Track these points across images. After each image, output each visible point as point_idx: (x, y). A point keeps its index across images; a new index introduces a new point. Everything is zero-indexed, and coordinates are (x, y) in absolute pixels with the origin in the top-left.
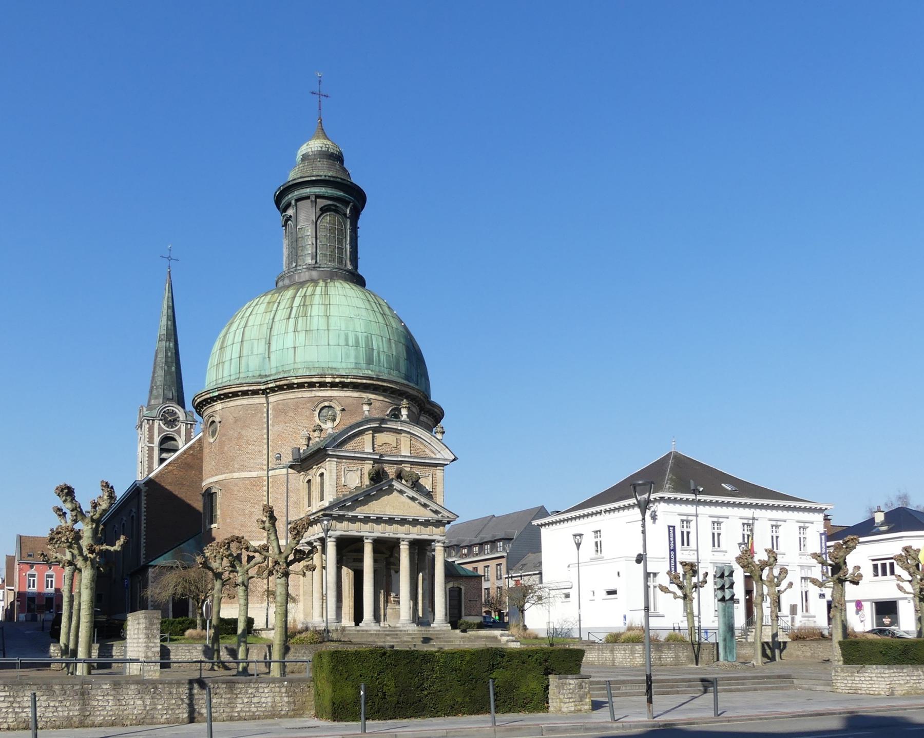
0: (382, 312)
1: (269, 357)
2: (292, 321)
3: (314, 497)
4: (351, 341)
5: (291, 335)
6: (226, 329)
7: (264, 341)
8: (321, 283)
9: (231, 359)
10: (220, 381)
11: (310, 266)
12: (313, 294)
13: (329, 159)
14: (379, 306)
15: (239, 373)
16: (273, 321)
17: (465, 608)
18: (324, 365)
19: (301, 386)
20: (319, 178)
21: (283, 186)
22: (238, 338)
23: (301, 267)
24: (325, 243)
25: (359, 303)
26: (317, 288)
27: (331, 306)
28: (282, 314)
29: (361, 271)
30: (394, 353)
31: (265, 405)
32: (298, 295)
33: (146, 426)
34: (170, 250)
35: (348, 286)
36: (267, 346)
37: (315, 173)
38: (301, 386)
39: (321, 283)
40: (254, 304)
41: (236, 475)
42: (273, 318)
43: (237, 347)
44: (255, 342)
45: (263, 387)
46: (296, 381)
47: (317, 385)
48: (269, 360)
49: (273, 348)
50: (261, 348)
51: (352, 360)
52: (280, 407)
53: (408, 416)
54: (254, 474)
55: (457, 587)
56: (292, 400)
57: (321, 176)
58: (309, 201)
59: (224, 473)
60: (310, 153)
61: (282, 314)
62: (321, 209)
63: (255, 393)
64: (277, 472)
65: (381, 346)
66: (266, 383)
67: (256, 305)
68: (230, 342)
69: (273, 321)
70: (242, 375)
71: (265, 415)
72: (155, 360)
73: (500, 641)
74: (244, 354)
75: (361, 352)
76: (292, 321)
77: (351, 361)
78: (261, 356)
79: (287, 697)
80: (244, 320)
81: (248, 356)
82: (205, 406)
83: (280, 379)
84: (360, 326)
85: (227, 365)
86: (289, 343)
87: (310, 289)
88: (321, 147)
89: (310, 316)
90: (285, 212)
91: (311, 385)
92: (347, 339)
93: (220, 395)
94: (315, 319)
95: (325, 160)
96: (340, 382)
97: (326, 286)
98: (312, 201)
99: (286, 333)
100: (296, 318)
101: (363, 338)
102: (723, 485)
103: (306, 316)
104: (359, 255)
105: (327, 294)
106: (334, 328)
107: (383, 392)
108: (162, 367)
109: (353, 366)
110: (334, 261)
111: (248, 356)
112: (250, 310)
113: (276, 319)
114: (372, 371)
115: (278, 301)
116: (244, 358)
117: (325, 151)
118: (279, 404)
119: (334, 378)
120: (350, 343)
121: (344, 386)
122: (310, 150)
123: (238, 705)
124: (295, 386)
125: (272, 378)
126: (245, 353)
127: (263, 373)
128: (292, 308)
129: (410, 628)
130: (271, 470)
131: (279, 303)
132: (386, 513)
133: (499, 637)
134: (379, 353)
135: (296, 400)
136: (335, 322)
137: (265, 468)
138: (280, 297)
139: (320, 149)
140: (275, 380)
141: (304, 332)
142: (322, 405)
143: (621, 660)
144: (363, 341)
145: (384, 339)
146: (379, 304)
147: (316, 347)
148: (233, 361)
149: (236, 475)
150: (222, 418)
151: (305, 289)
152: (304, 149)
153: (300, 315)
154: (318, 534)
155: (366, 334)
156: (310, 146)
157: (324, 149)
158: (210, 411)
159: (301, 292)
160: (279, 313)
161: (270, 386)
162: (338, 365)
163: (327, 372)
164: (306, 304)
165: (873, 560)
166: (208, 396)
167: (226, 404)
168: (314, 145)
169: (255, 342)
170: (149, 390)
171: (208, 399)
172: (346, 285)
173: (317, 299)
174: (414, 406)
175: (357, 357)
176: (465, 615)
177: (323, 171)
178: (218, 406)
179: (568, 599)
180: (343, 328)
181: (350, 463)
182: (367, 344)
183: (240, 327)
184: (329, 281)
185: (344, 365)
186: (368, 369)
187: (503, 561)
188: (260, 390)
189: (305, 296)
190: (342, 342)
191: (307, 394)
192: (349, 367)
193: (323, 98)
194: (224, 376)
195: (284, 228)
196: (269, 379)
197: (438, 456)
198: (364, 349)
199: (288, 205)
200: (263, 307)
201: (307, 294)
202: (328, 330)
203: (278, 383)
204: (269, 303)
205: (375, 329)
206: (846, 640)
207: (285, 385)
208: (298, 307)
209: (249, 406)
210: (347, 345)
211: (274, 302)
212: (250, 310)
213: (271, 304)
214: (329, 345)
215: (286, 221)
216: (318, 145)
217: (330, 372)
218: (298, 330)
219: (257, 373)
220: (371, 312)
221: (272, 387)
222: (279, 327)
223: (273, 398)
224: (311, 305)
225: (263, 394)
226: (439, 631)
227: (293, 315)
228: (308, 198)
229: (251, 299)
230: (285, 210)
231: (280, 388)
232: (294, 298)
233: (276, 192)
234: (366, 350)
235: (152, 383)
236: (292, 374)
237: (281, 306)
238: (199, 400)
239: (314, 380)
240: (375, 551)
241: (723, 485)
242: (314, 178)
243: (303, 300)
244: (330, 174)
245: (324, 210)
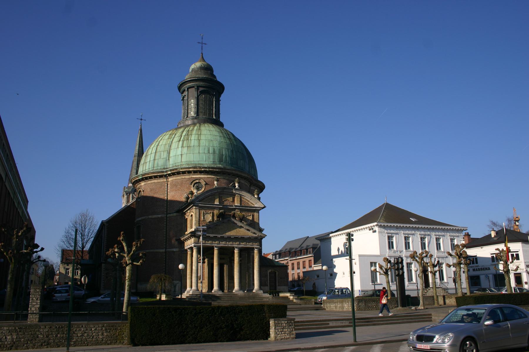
0: (229, 138)
1: (169, 160)
2: (181, 143)
3: (189, 227)
4: (211, 151)
5: (180, 149)
6: (149, 147)
7: (167, 152)
8: (198, 125)
9: (150, 161)
10: (144, 172)
11: (194, 117)
12: (193, 130)
13: (205, 70)
14: (227, 135)
15: (154, 167)
16: (172, 143)
17: (278, 282)
18: (196, 163)
19: (184, 173)
20: (199, 78)
21: (181, 82)
22: (154, 151)
23: (189, 118)
24: (202, 107)
25: (216, 133)
26: (195, 127)
27: (202, 135)
28: (176, 139)
29: (221, 120)
30: (235, 157)
31: (166, 182)
32: (185, 130)
33: (125, 196)
34: (142, 116)
35: (211, 126)
36: (168, 154)
37: (197, 76)
38: (184, 173)
39: (198, 125)
40: (164, 135)
41: (150, 217)
42: (172, 141)
43: (153, 155)
44: (162, 153)
45: (165, 174)
46: (181, 170)
47: (192, 172)
48: (169, 161)
49: (171, 155)
50: (165, 155)
51: (212, 160)
52: (174, 183)
53: (239, 186)
54: (160, 216)
55: (274, 272)
56: (180, 180)
57: (200, 77)
58: (194, 88)
59: (144, 216)
60: (196, 68)
61: (176, 139)
62: (200, 92)
63: (161, 176)
64: (172, 215)
65: (227, 153)
66: (167, 171)
67: (164, 135)
68: (150, 153)
69: (172, 143)
70: (155, 168)
71: (166, 187)
72: (132, 165)
73: (289, 299)
74: (156, 158)
75: (216, 156)
76: (181, 143)
77: (211, 161)
78: (165, 159)
79: (106, 332)
80: (158, 142)
81: (158, 159)
82: (137, 183)
83: (173, 170)
84: (216, 144)
85: (148, 164)
86: (179, 152)
87: (191, 128)
88: (201, 65)
89: (190, 140)
90: (183, 94)
91: (189, 172)
92: (209, 150)
93: (143, 178)
94: (193, 141)
95: (203, 71)
96: (204, 171)
97: (200, 126)
98: (195, 88)
99: (178, 148)
100: (183, 141)
101: (218, 150)
102: (410, 218)
103: (188, 140)
104: (221, 112)
105: (200, 129)
106: (203, 145)
107: (223, 174)
108: (135, 169)
109: (212, 163)
110: (206, 115)
111: (158, 159)
112: (161, 138)
113: (173, 142)
114: (222, 165)
115: (175, 133)
116: (156, 160)
117: (203, 67)
118: (173, 182)
119: (201, 168)
120: (211, 152)
121: (201, 172)
122: (196, 66)
123: (74, 338)
124: (181, 173)
125: (169, 169)
126: (157, 158)
127: (166, 167)
128: (181, 136)
129: (240, 293)
130: (169, 214)
131: (176, 134)
132: (237, 235)
133: (289, 297)
134: (226, 157)
135: (182, 179)
136: (203, 143)
137: (165, 213)
138: (176, 132)
139: (200, 66)
140: (171, 170)
141: (187, 147)
142: (195, 182)
143: (347, 307)
144: (218, 151)
145: (229, 150)
146: (228, 134)
147: (192, 154)
148: (151, 162)
149: (150, 217)
150: (144, 189)
151: (189, 128)
152: (193, 66)
153: (185, 139)
154: (190, 245)
155: (219, 148)
156: (196, 65)
157: (202, 66)
158: (139, 186)
159: (187, 129)
160: (175, 139)
161: (168, 173)
162: (204, 163)
163: (197, 166)
164: (189, 134)
165: (491, 254)
166: (137, 179)
167: (147, 182)
168: (198, 64)
169: (162, 153)
170: (128, 179)
171: (138, 180)
172: (211, 126)
173: (194, 132)
174: (246, 182)
175: (214, 159)
176: (278, 286)
177: (202, 75)
178: (143, 184)
179: (331, 277)
180: (207, 145)
181: (206, 210)
182: (219, 152)
183: (155, 146)
184: (202, 124)
185: (207, 162)
186: (220, 164)
187: (312, 259)
188: (164, 175)
189: (188, 131)
190: (206, 151)
191: (187, 177)
192: (210, 163)
193: (203, 45)
194: (146, 169)
195: (182, 101)
196: (167, 170)
197: (256, 206)
198: (218, 155)
199: (184, 91)
200: (167, 137)
201: (190, 130)
202: (199, 146)
203: (172, 172)
204: (170, 134)
205: (225, 146)
206: (472, 294)
207: (176, 172)
208: (184, 136)
209: (158, 183)
210: (209, 153)
211: (173, 134)
212: (161, 138)
213: (172, 135)
214: (199, 153)
215: (183, 98)
216: (199, 64)
217: (199, 166)
218: (184, 146)
219: (163, 167)
220: (222, 138)
221: (169, 174)
222: (174, 146)
223: (170, 179)
224: (191, 135)
225: (165, 177)
226: (256, 294)
227: (182, 140)
228: (193, 87)
229: (163, 133)
230: (182, 93)
231: (173, 174)
232: (183, 132)
233: (178, 85)
234: (219, 155)
235: (130, 176)
236: (179, 167)
237: (176, 136)
238: (133, 181)
239: (191, 170)
240: (240, 256)
241: (410, 218)
242: (196, 78)
243: (187, 133)
244: (204, 77)
245: (202, 92)
